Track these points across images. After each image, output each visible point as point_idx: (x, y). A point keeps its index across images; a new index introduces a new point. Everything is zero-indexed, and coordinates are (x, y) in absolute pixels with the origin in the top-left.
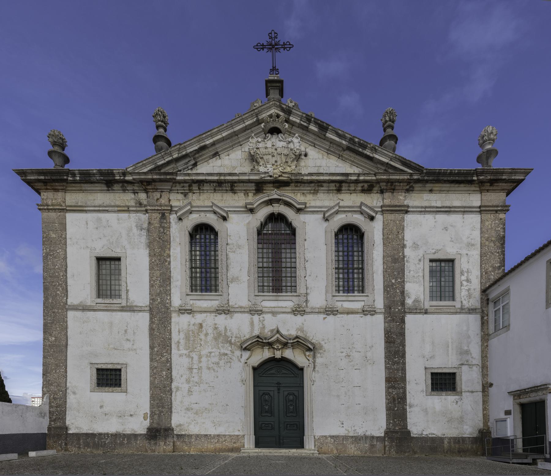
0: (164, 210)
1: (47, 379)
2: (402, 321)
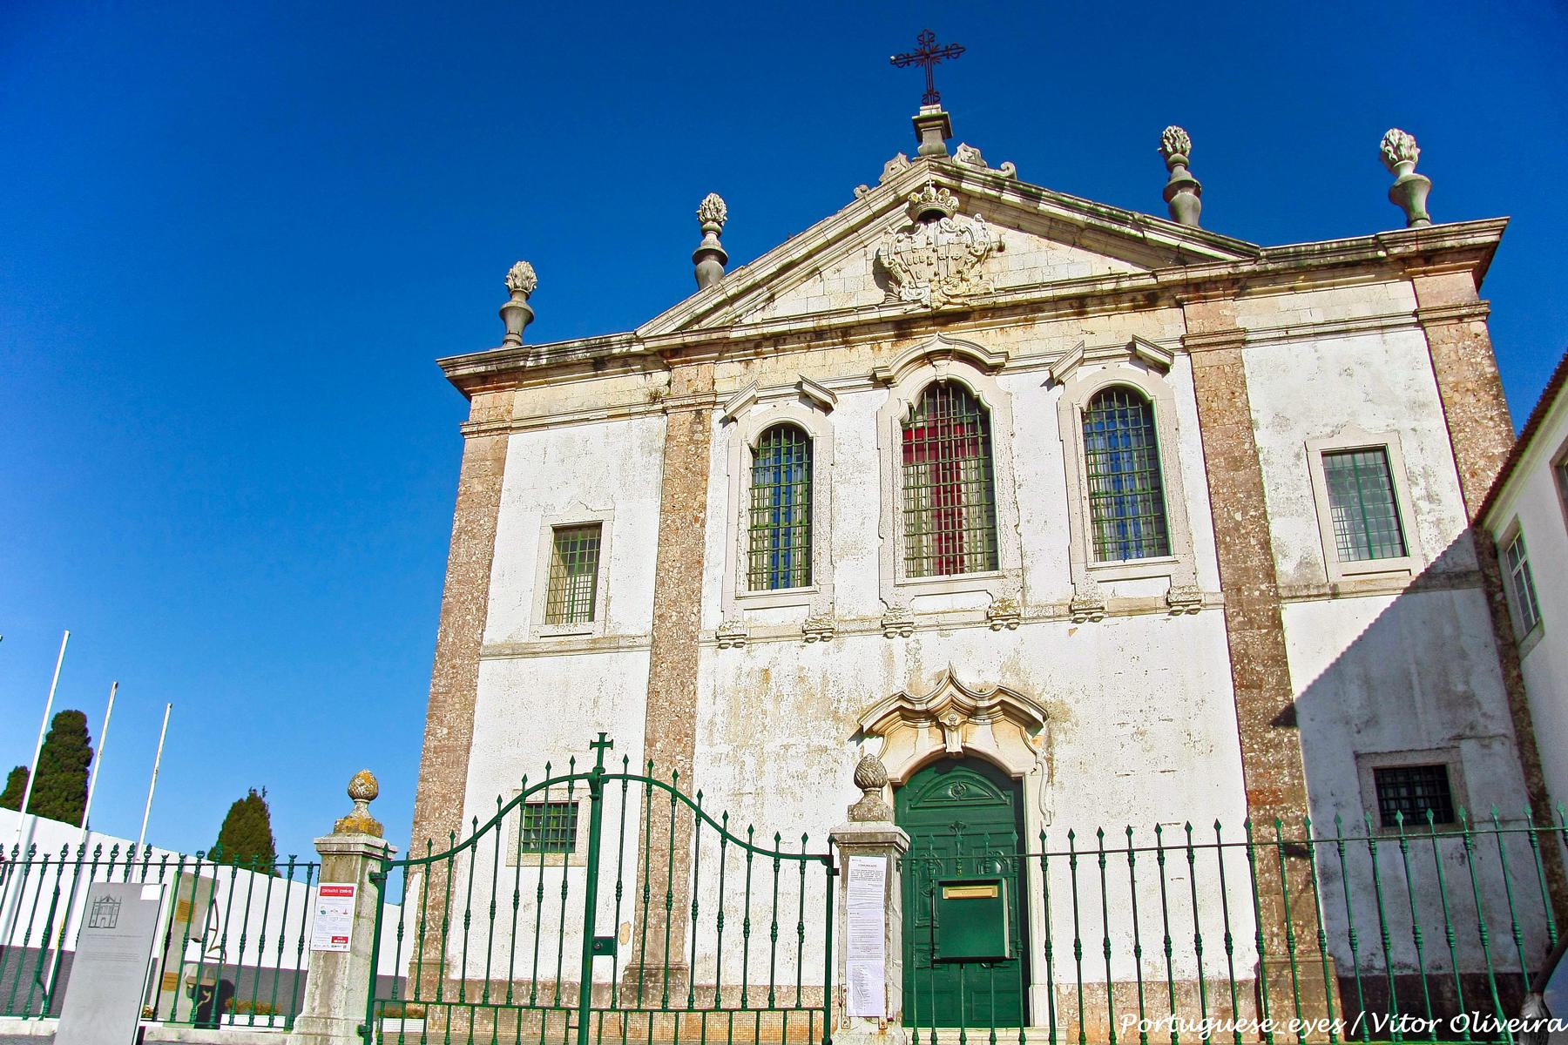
0: (700, 404)
1: (422, 834)
2: (1273, 622)
